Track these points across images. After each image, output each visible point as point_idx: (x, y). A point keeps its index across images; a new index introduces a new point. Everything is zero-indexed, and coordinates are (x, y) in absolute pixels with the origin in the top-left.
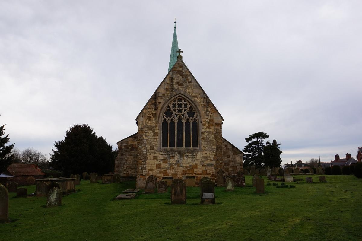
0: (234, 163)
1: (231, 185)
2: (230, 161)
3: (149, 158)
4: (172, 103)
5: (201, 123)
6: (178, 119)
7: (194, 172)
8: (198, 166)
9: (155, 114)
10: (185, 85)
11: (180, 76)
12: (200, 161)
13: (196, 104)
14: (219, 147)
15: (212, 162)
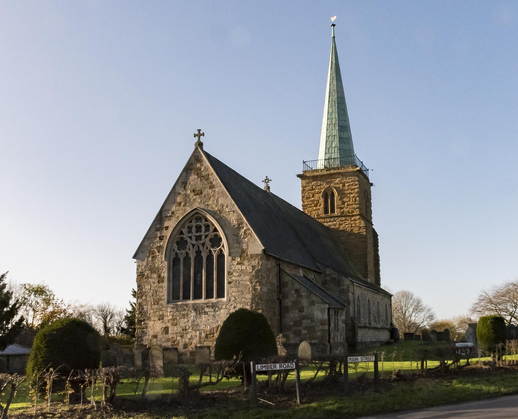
0: (309, 321)
2: (304, 318)
3: (153, 319)
6: (196, 252)
10: (205, 192)
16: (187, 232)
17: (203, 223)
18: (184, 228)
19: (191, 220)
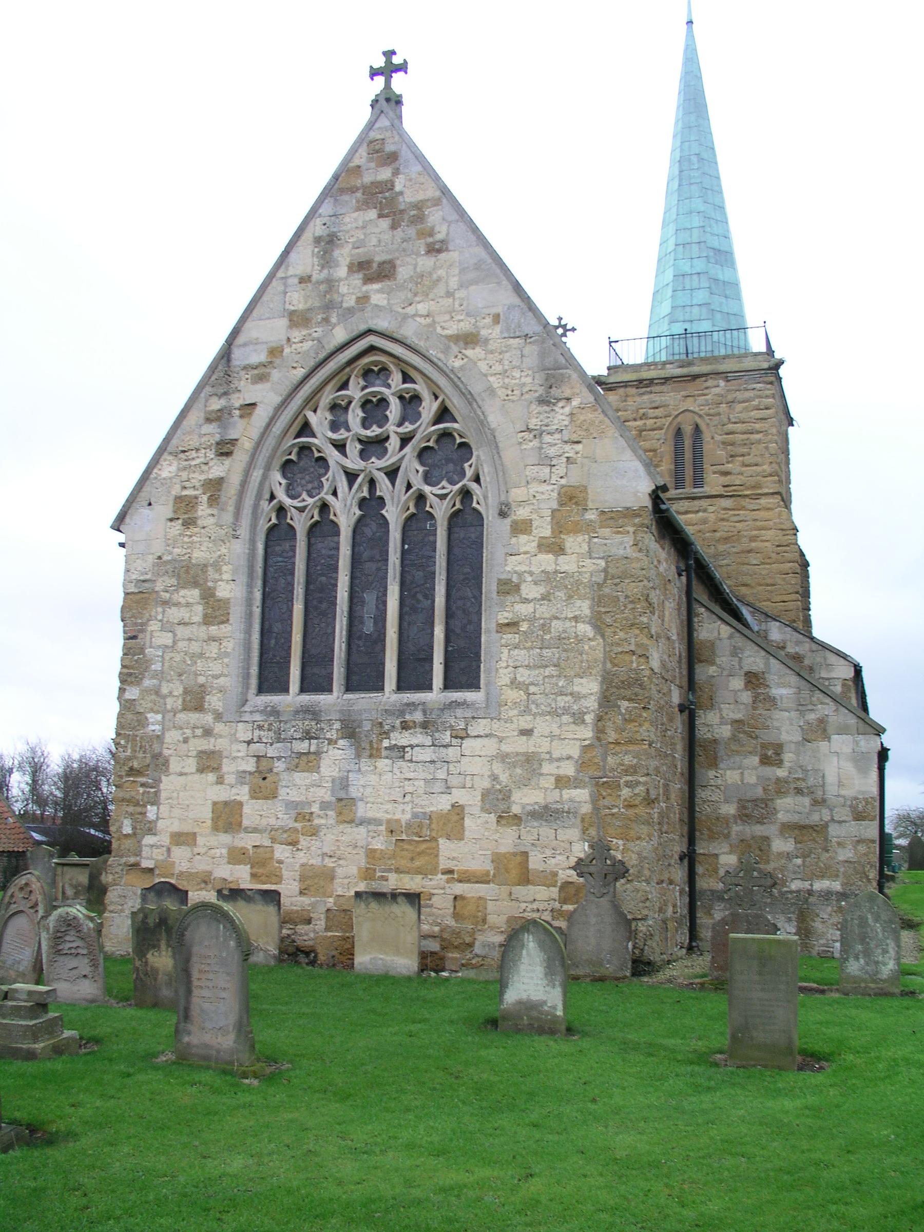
0: (806, 801)
1: (539, 970)
2: (781, 787)
3: (174, 766)
4: (327, 397)
5: (503, 514)
6: (362, 503)
7: (443, 864)
8: (468, 822)
9: (220, 481)
10: (404, 272)
11: (380, 216)
12: (487, 784)
13: (476, 388)
14: (627, 684)
15: (568, 794)
16: (326, 423)
17: (393, 390)
18: (315, 411)
19: (345, 378)
